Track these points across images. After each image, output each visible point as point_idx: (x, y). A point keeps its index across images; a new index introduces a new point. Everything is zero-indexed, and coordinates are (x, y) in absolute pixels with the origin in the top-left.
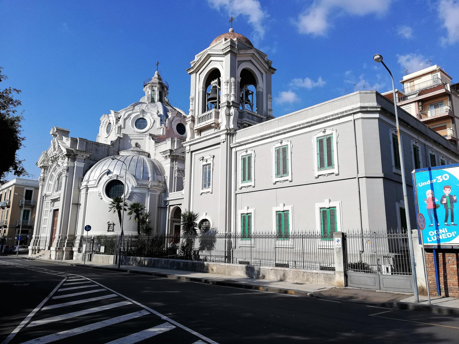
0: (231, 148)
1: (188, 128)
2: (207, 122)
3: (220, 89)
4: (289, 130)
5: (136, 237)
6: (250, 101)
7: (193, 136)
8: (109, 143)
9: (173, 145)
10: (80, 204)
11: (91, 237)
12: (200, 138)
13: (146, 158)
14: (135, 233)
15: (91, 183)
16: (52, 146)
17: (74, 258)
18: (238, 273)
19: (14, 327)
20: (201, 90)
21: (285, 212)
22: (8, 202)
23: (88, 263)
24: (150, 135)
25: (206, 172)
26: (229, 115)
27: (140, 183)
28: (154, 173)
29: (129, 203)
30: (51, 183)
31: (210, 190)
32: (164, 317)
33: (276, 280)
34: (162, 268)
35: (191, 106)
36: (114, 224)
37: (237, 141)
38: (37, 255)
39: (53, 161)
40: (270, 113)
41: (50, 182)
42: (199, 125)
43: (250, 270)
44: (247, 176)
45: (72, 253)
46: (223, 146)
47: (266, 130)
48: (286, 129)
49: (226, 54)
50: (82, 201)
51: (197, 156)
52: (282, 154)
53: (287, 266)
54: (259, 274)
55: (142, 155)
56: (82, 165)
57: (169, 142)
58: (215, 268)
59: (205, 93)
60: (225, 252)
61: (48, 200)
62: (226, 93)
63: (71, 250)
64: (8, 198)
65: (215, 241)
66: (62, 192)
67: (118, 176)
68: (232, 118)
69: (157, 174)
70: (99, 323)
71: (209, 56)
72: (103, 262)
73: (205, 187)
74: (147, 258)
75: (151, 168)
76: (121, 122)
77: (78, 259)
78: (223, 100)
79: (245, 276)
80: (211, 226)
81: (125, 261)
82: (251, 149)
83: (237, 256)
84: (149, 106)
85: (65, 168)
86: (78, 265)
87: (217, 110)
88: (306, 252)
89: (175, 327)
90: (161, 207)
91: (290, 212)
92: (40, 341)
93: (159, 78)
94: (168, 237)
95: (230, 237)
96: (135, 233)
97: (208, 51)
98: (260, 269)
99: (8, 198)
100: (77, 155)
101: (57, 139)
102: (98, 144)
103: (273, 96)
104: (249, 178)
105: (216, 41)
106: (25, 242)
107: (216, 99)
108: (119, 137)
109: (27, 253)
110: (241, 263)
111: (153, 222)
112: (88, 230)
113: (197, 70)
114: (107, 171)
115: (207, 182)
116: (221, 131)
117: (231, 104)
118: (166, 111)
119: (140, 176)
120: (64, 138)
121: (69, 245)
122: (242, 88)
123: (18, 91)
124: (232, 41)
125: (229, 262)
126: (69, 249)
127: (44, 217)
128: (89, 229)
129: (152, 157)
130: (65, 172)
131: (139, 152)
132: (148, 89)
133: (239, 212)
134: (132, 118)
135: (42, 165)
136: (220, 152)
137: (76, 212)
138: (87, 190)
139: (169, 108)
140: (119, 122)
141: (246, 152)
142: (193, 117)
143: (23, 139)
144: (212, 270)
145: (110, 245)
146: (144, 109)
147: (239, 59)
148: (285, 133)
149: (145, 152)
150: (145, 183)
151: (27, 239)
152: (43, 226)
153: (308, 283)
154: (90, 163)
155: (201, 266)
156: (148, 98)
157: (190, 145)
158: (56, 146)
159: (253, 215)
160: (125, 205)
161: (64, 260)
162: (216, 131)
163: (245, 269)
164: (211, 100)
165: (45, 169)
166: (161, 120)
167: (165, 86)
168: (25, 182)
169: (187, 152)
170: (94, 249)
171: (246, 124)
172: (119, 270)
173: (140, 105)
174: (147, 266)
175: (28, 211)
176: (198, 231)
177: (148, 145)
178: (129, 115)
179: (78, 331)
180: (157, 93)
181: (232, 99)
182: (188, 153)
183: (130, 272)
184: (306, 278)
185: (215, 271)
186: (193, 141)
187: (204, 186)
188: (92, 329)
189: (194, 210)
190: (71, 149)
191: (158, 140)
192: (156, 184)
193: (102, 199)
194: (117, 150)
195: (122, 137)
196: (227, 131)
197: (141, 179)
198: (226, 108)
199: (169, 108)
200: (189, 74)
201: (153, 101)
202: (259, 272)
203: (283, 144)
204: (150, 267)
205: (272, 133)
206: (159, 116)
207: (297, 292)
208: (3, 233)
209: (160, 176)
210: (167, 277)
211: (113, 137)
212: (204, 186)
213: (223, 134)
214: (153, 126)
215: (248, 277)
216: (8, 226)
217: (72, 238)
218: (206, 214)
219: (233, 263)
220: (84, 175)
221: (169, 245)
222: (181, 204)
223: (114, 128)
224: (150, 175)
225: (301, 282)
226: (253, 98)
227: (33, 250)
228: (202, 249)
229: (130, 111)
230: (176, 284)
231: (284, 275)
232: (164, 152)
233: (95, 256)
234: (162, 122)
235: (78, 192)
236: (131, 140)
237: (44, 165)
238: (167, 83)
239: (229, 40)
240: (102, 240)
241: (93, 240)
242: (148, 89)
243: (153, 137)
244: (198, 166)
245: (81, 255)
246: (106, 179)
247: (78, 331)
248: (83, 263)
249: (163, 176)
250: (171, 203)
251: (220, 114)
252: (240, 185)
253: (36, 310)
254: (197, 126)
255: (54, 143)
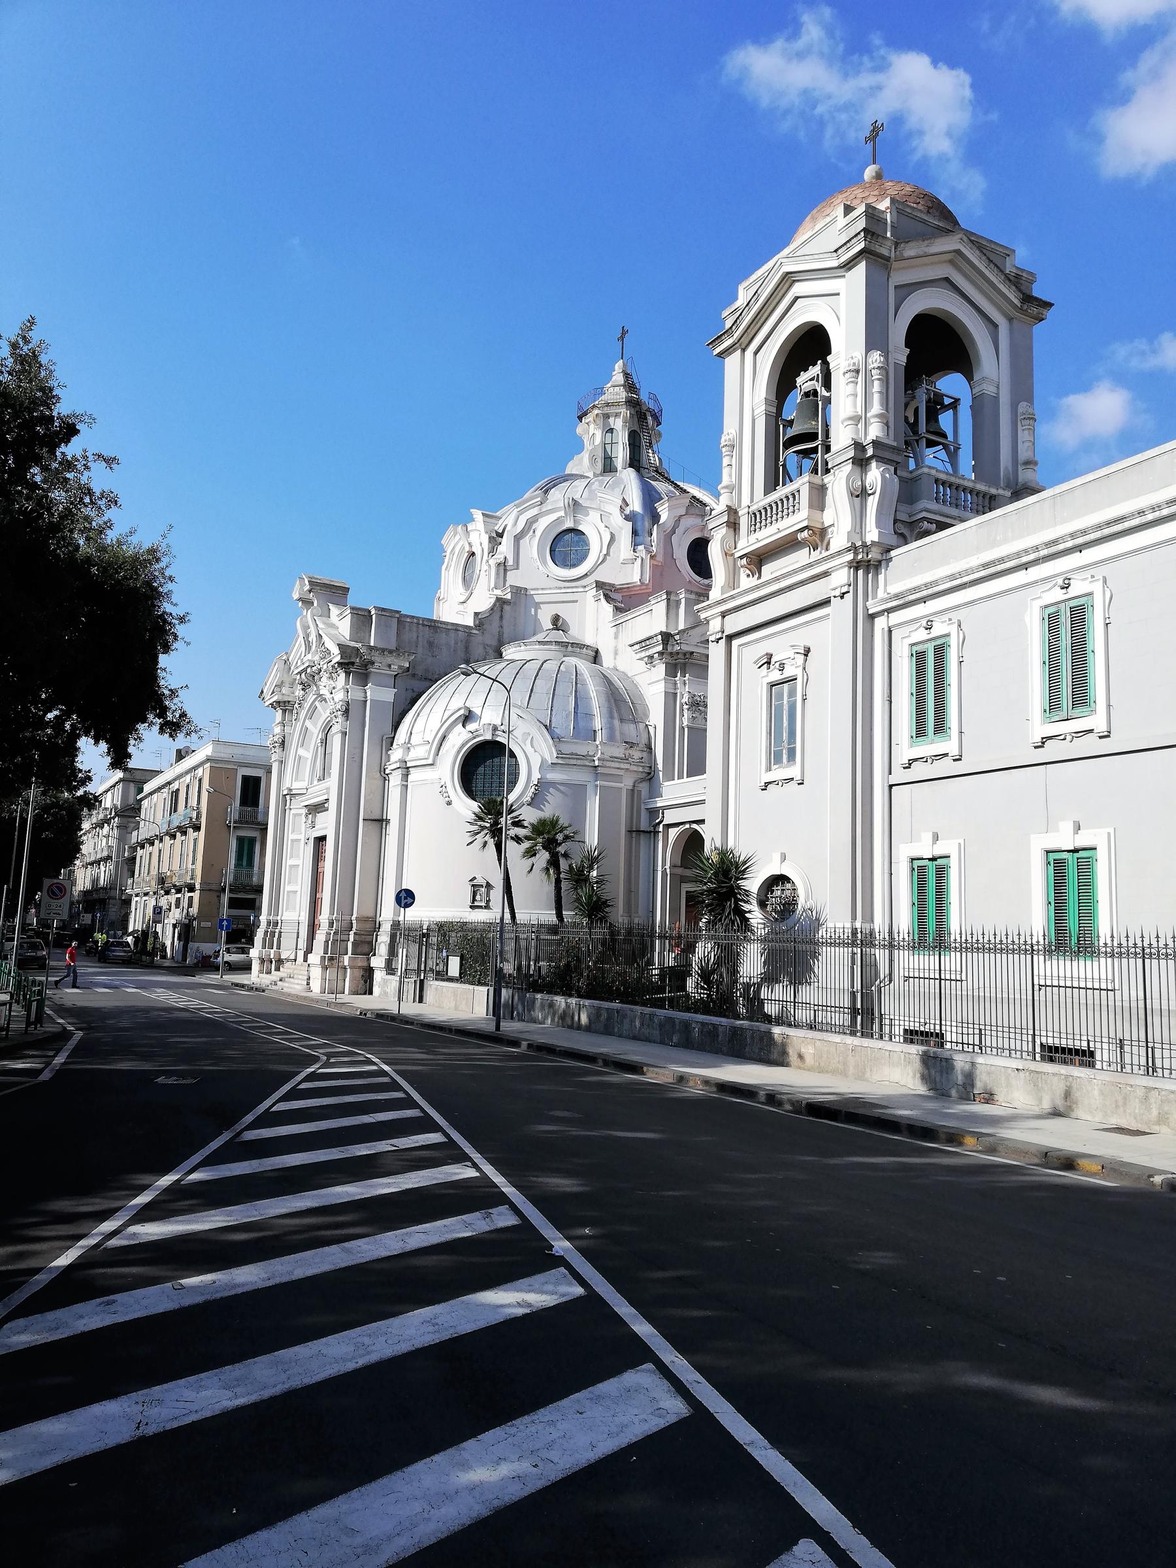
0: (872, 617)
1: (715, 552)
2: (782, 524)
3: (828, 401)
4: (1098, 535)
5: (553, 930)
6: (944, 436)
7: (733, 582)
8: (469, 621)
9: (672, 612)
10: (388, 821)
11: (421, 927)
12: (757, 587)
13: (584, 667)
14: (550, 917)
15: (419, 753)
16: (301, 639)
17: (376, 989)
18: (887, 1074)
19: (69, 1243)
20: (761, 409)
21: (1081, 854)
22: (194, 815)
23: (410, 1008)
24: (600, 585)
25: (780, 708)
26: (860, 494)
27: (567, 749)
28: (611, 717)
29: (530, 816)
30: (304, 753)
31: (794, 771)
32: (561, 1245)
33: (1036, 1110)
34: (635, 1038)
35: (725, 471)
36: (489, 886)
37: (894, 589)
38: (275, 975)
39: (305, 687)
40: (1025, 475)
41: (301, 752)
42: (753, 538)
43: (937, 1068)
44: (931, 716)
45: (369, 972)
46: (841, 610)
47: (1005, 541)
48: (1084, 532)
49: (849, 265)
50: (393, 813)
51: (748, 652)
52: (1069, 633)
53: (1085, 1057)
54: (973, 1086)
55: (573, 654)
56: (387, 695)
57: (658, 607)
58: (808, 1051)
59: (775, 418)
60: (853, 994)
61: (297, 808)
62: (849, 412)
63: (365, 964)
64: (193, 802)
65: (815, 955)
66: (333, 782)
67: (495, 728)
68: (872, 503)
69: (622, 720)
70: (334, 1248)
71: (789, 279)
72: (456, 1008)
73: (778, 760)
74: (587, 1002)
75: (603, 699)
76: (505, 548)
77: (386, 993)
78: (841, 437)
79: (922, 1089)
80: (801, 902)
81: (520, 1007)
82: (945, 618)
83: (900, 1009)
84: (596, 486)
85: (338, 707)
86: (381, 1016)
87: (817, 479)
88: (1156, 1006)
89: (579, 1291)
90: (638, 831)
91: (1102, 856)
92: (113, 1308)
93: (630, 386)
94: (663, 937)
95: (868, 940)
96: (550, 917)
97: (784, 262)
98: (973, 1064)
99: (193, 802)
100: (373, 663)
101: (313, 615)
102: (434, 626)
103: (1038, 409)
104: (940, 727)
105: (815, 220)
106: (242, 936)
107: (813, 437)
108: (498, 599)
109: (246, 967)
110: (911, 1036)
111: (612, 878)
112: (407, 906)
113: (745, 340)
114: (462, 712)
115: (783, 743)
116: (832, 556)
117: (870, 452)
118: (650, 498)
119: (567, 727)
120: (334, 610)
121: (359, 951)
122: (914, 389)
123: (110, 461)
124: (872, 214)
125: (867, 1034)
126: (361, 961)
127: (288, 862)
128: (409, 900)
129: (607, 661)
130: (340, 720)
131: (564, 645)
132: (592, 426)
133: (904, 852)
134: (538, 533)
135: (275, 698)
136: (831, 633)
137: (376, 845)
138: (406, 776)
139: (661, 487)
140: (500, 548)
141: (929, 628)
142: (732, 511)
143: (182, 620)
144: (801, 1057)
145: (474, 951)
146: (577, 497)
147: (899, 277)
148: (1079, 548)
149: (582, 646)
150: (582, 749)
151: (248, 925)
152: (287, 887)
153: (1164, 1129)
154: (413, 687)
155: (761, 1039)
156: (593, 460)
157: (723, 615)
158: (313, 637)
159: (954, 863)
160: (518, 824)
161: (346, 997)
162: (816, 555)
163: (917, 1064)
164: (796, 442)
165: (284, 711)
166: (635, 533)
167: (648, 410)
168: (238, 750)
169: (712, 638)
170: (430, 964)
171: (930, 521)
172: (495, 1038)
173: (567, 484)
174: (588, 1029)
175: (252, 841)
176: (756, 917)
177: (593, 620)
178: (531, 522)
179: (248, 1276)
180: (622, 437)
181: (875, 431)
182: (717, 641)
183: (530, 1046)
184: (1155, 1112)
185: (809, 1060)
186: (732, 597)
187: (775, 758)
188: (300, 1273)
189: (741, 847)
190: (353, 644)
191: (623, 600)
192: (619, 751)
193: (449, 803)
194: (494, 643)
195: (509, 597)
196: (856, 554)
197: (570, 736)
198: (848, 467)
199: (661, 487)
200: (720, 355)
201: (608, 467)
202: (970, 1078)
203: (1074, 591)
204: (596, 1032)
205: (1026, 551)
206: (627, 518)
207: (1110, 1167)
208: (186, 906)
209: (632, 726)
210: (643, 1073)
211: (483, 601)
212: (775, 758)
213: (841, 566)
214: (608, 554)
215: (931, 1093)
216: (198, 886)
217: (369, 926)
218: (784, 858)
219: (881, 1037)
220: (396, 727)
221: (670, 960)
222: (702, 822)
223: (485, 569)
224: (598, 724)
225: (1134, 1126)
226: (958, 425)
227: (262, 961)
228: (770, 978)
229: (533, 506)
230: (666, 1105)
231: (1067, 1095)
232: (644, 643)
233: (434, 987)
234: (639, 539)
235: (380, 782)
236: (537, 606)
237: (281, 698)
238: (656, 400)
239: (861, 209)
240: (454, 938)
241: (427, 935)
242: (592, 426)
243: (607, 591)
244: (753, 686)
245: (394, 981)
246: (460, 740)
247: (248, 1276)
248: (393, 1008)
249: (642, 726)
250: (670, 817)
251: (829, 492)
252: (905, 750)
253: (167, 1180)
254: (749, 542)
255: (306, 628)
